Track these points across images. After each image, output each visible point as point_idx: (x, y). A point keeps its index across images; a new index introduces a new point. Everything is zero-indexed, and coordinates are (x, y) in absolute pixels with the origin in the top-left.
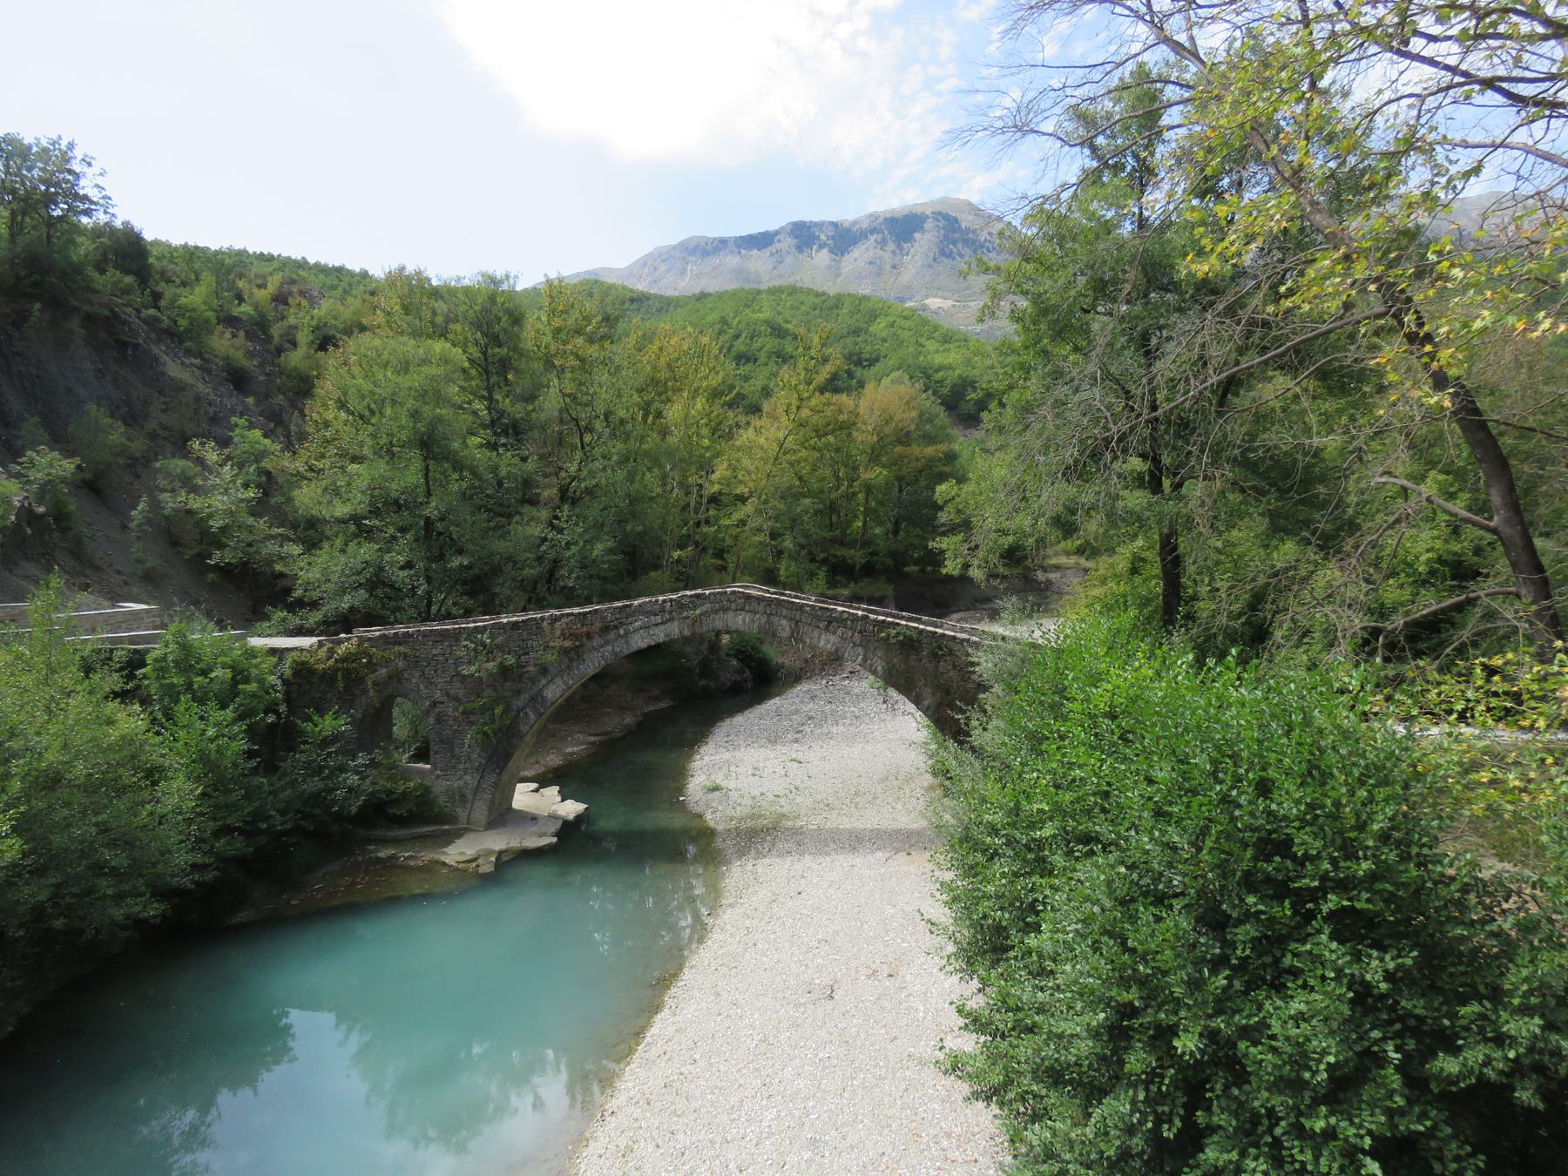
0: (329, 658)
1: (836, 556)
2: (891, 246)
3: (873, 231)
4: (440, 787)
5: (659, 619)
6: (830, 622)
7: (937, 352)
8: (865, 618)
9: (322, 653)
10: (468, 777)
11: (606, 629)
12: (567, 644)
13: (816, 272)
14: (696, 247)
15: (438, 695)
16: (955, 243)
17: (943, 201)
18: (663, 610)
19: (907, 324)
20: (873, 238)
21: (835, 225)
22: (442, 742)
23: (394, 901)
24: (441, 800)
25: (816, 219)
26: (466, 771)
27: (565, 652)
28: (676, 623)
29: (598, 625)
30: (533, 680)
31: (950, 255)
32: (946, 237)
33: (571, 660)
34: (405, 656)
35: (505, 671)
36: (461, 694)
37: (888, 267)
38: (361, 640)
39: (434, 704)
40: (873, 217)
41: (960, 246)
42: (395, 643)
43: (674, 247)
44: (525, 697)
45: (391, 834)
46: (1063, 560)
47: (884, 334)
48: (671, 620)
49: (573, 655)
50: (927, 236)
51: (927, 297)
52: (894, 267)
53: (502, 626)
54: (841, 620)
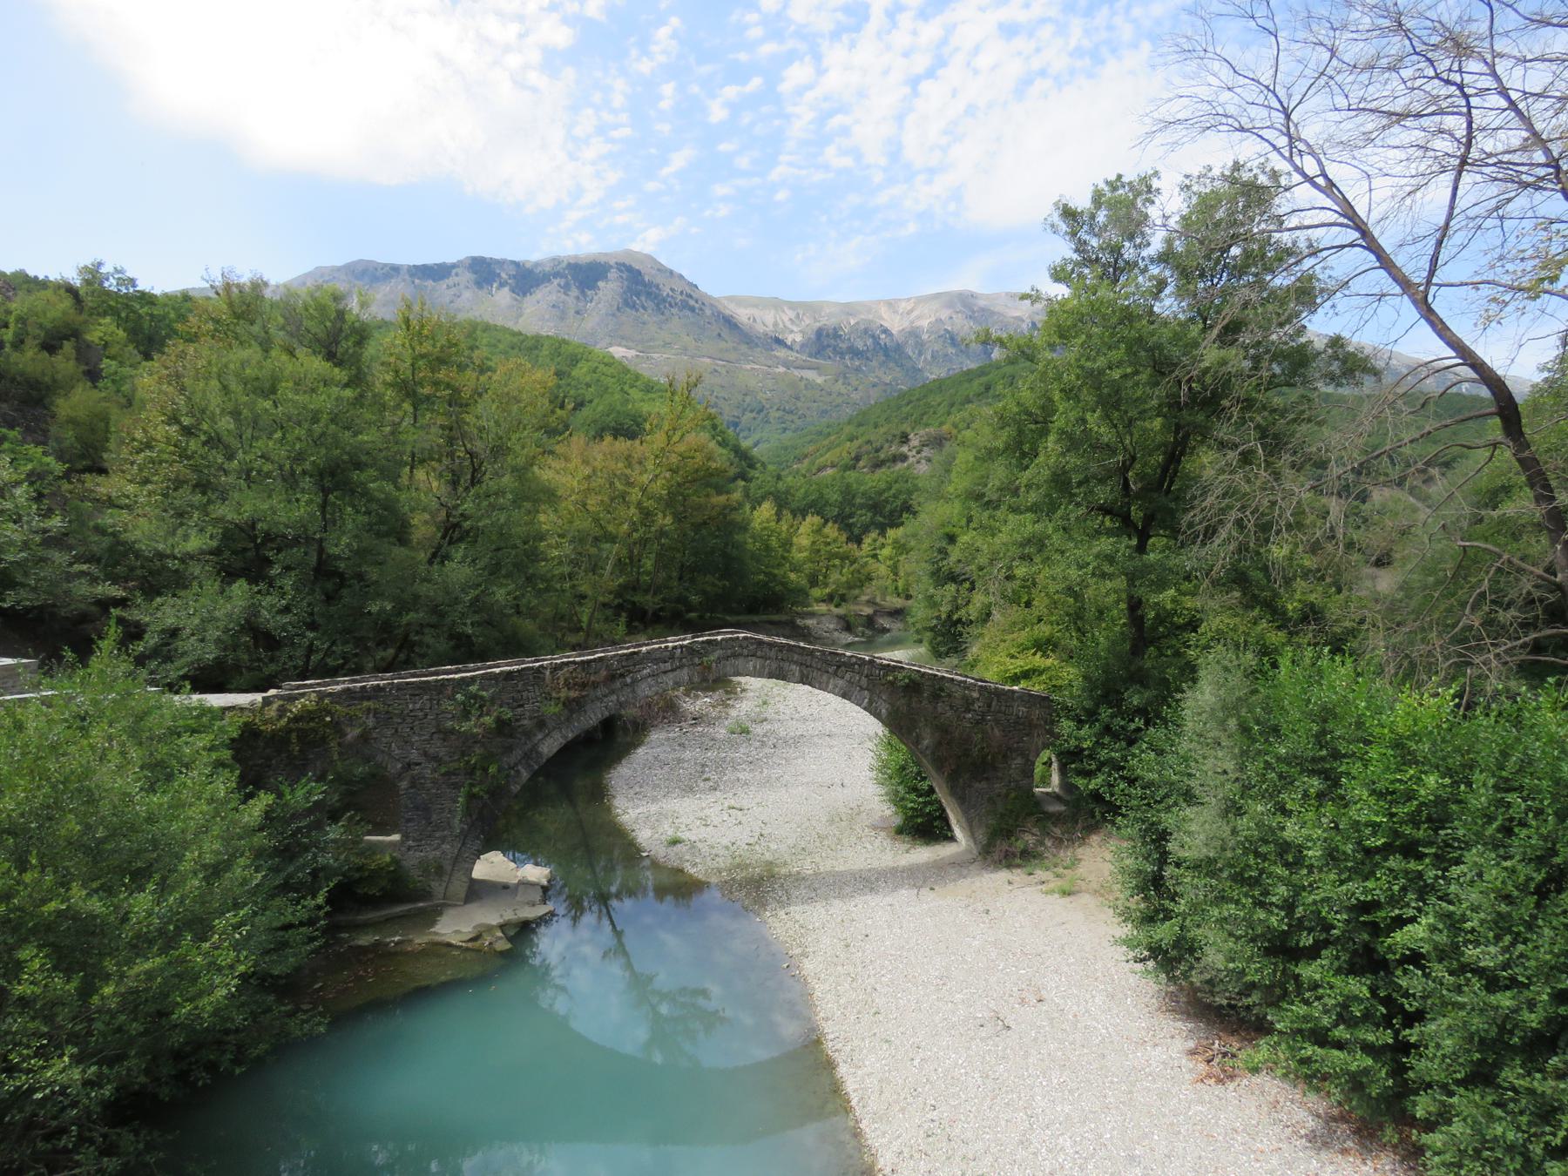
0: (280, 717)
1: (634, 603)
2: (575, 292)
3: (556, 275)
4: (411, 860)
5: (668, 666)
9: (272, 712)
10: (446, 847)
11: (612, 678)
12: (573, 694)
13: (496, 307)
14: (364, 272)
15: (414, 755)
16: (638, 295)
18: (672, 657)
19: (610, 371)
20: (556, 282)
22: (417, 808)
23: (422, 994)
24: (415, 874)
25: (497, 255)
26: (443, 839)
28: (685, 670)
29: (604, 673)
30: (528, 734)
31: (633, 307)
33: (572, 711)
34: (376, 712)
35: (503, 726)
36: (442, 752)
37: (572, 312)
39: (409, 766)
40: (556, 261)
42: (363, 698)
43: (339, 269)
44: (518, 754)
45: (362, 917)
46: (823, 608)
47: (588, 379)
48: (681, 667)
49: (574, 707)
50: (611, 285)
51: (611, 345)
52: (577, 313)
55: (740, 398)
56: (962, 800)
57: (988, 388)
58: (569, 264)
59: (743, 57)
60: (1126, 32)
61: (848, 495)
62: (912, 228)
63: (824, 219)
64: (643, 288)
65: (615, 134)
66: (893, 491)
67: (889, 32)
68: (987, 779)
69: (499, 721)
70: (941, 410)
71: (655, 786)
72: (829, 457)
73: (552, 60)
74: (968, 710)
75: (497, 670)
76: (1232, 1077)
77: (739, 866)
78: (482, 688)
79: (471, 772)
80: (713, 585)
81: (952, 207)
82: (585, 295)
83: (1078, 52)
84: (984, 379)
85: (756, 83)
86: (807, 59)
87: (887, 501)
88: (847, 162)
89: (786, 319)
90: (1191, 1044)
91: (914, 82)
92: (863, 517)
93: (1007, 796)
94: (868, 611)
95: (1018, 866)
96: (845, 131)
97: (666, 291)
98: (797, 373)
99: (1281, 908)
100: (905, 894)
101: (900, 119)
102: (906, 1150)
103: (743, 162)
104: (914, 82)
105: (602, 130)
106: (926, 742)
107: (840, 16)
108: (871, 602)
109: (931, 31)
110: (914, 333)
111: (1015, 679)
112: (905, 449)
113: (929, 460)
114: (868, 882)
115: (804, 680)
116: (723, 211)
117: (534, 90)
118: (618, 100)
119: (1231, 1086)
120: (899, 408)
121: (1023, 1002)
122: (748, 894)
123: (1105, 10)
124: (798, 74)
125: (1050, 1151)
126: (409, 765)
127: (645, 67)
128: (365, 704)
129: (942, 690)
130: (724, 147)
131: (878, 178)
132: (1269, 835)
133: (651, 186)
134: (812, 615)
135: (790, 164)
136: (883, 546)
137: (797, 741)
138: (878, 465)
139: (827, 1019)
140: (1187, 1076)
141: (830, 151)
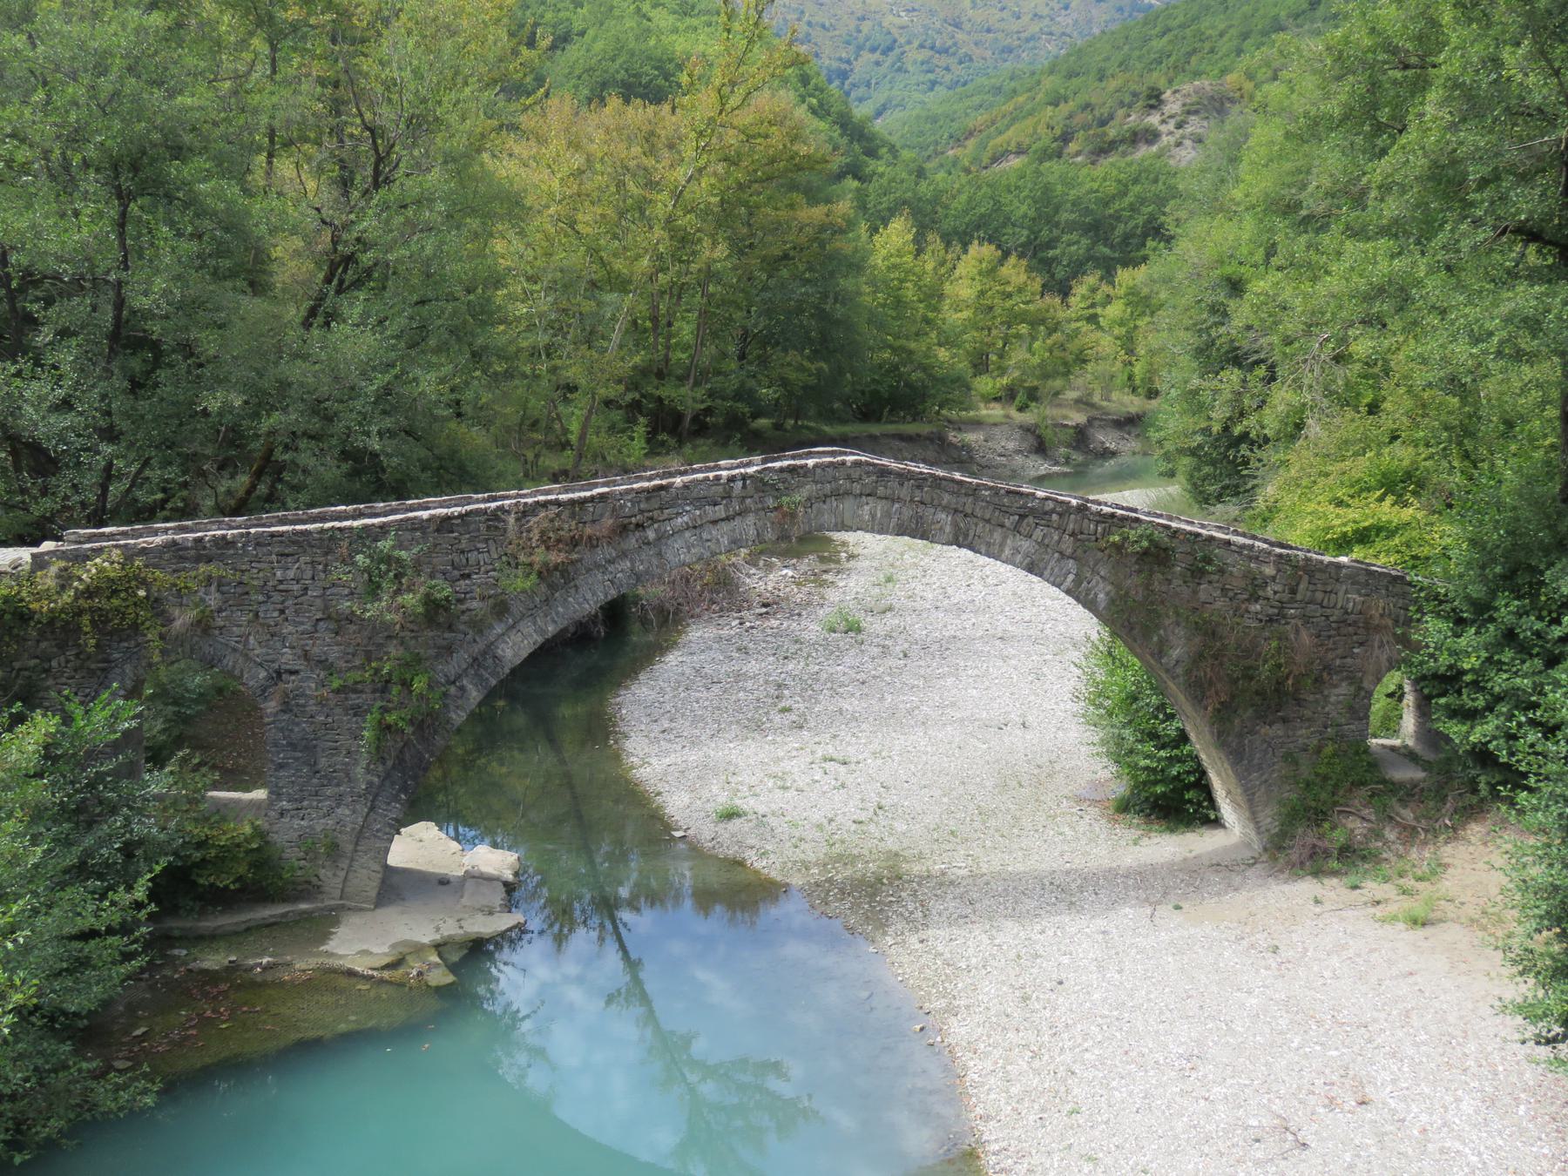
4: (286, 834)
5: (720, 511)
6: (1022, 517)
7: (675, 31)
9: (48, 579)
10: (343, 811)
11: (623, 530)
12: (556, 557)
15: (288, 658)
22: (293, 746)
24: (292, 855)
27: (546, 573)
29: (608, 522)
30: (479, 626)
33: (553, 587)
35: (435, 612)
36: (334, 653)
38: (130, 554)
42: (198, 559)
44: (461, 658)
46: (995, 412)
48: (741, 513)
49: (556, 579)
53: (420, 525)
56: (1237, 755)
68: (1285, 720)
70: (1225, 46)
71: (696, 720)
72: (1013, 135)
74: (1254, 598)
77: (839, 857)
79: (384, 687)
87: (1118, 218)
94: (1078, 418)
95: (1334, 873)
100: (1129, 914)
106: (1175, 653)
108: (1083, 403)
111: (1344, 544)
112: (1154, 119)
113: (1199, 140)
114: (1067, 892)
121: (1331, 1103)
126: (279, 673)
129: (1208, 561)
134: (977, 424)
136: (1108, 299)
137: (944, 647)
138: (1103, 149)
139: (986, 1118)
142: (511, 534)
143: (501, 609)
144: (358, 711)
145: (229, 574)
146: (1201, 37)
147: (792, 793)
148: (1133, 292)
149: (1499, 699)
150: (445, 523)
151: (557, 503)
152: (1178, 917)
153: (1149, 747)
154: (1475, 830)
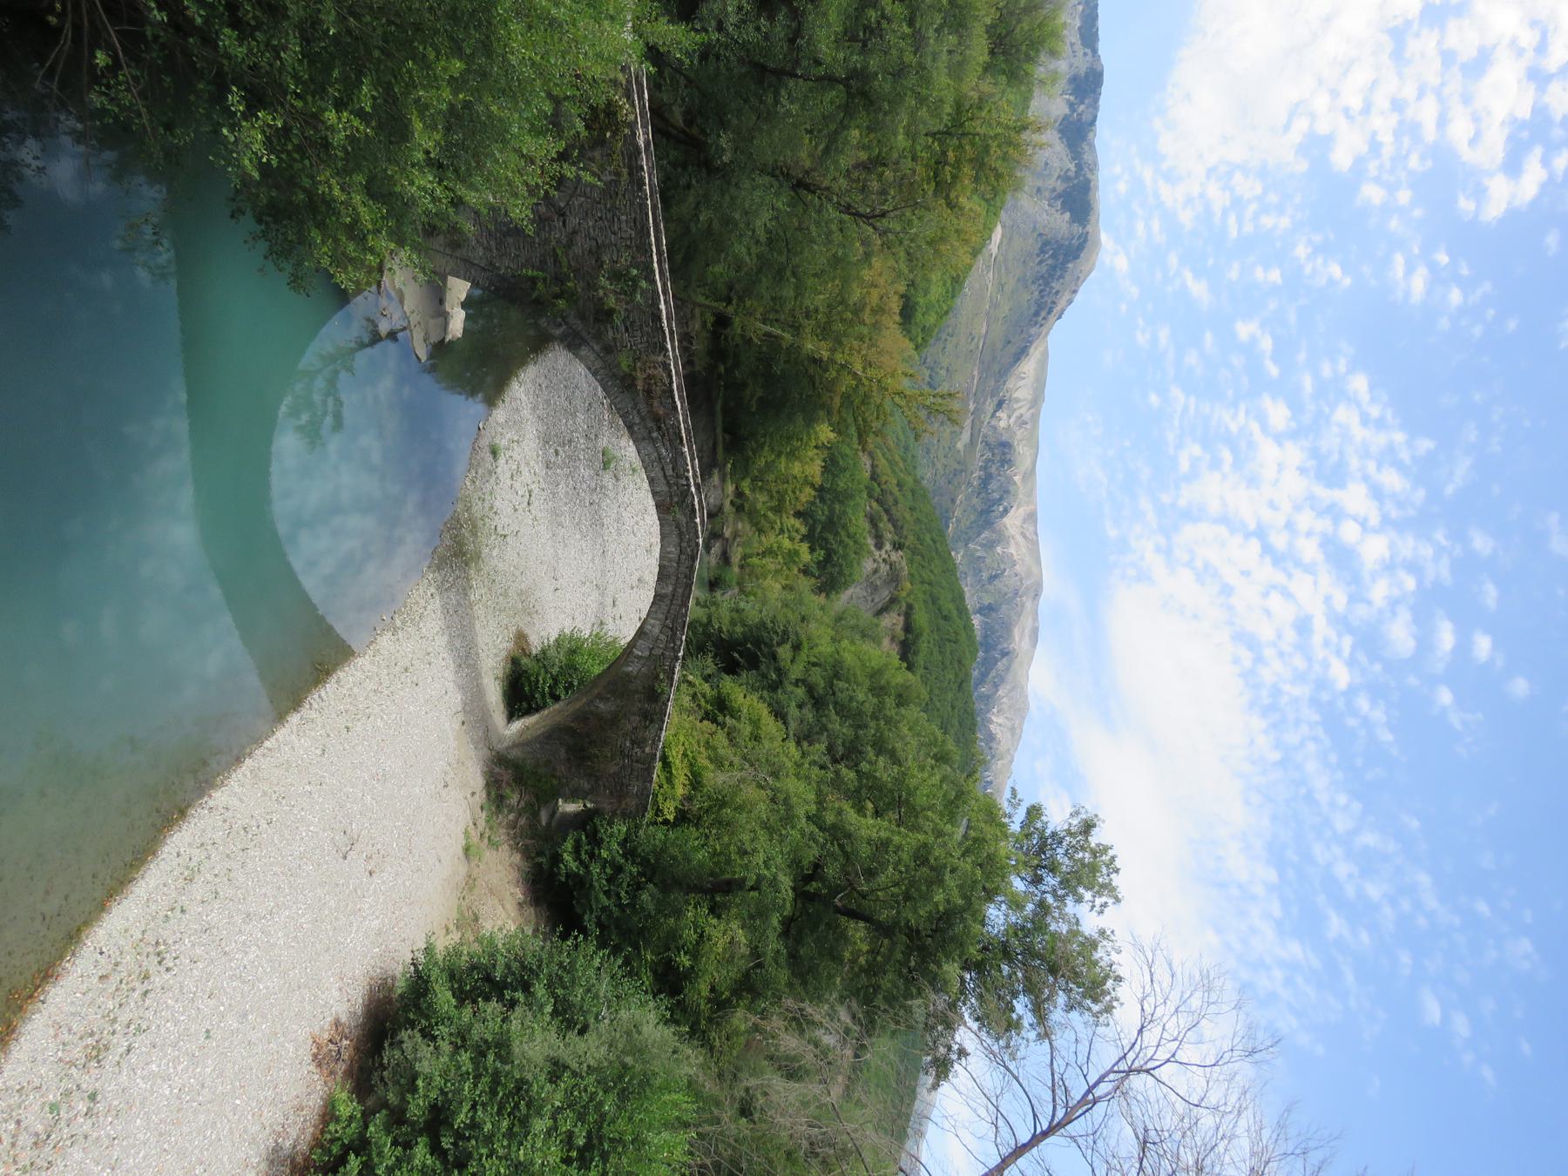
2: (1060, 186)
3: (1079, 167)
5: (670, 472)
8: (677, 658)
10: (481, 251)
11: (657, 420)
15: (573, 221)
16: (1054, 256)
17: (1097, 243)
18: (678, 476)
20: (1072, 167)
21: (1093, 122)
25: (1103, 101)
26: (487, 249)
28: (665, 488)
30: (598, 336)
31: (1042, 251)
32: (1060, 246)
33: (623, 379)
34: (617, 183)
36: (577, 250)
37: (1039, 184)
39: (562, 214)
41: (1050, 262)
42: (630, 168)
44: (578, 325)
46: (730, 488)
50: (1065, 226)
51: (1003, 227)
52: (1039, 190)
53: (656, 303)
54: (673, 638)
55: (945, 365)
56: (551, 736)
57: (946, 618)
58: (1089, 181)
59: (1302, 356)
60: (1292, 738)
61: (843, 497)
62: (1113, 533)
63: (1127, 443)
64: (1060, 261)
65: (1232, 219)
66: (846, 540)
67: (1312, 508)
68: (569, 760)
69: (611, 312)
70: (926, 574)
71: (547, 402)
72: (882, 463)
73: (1317, 146)
74: (633, 742)
75: (662, 306)
76: (319, 1065)
77: (475, 526)
78: (643, 292)
79: (559, 279)
80: (752, 396)
81: (1132, 572)
82: (1056, 198)
83: (1276, 691)
84: (955, 613)
85: (1274, 371)
86: (1293, 425)
87: (837, 534)
88: (1184, 466)
89: (1023, 411)
90: (344, 1019)
91: (1260, 533)
92: (821, 514)
93: (554, 776)
94: (727, 533)
95: (489, 794)
96: (1216, 464)
97: (1056, 285)
98: (968, 422)
99: (473, 1118)
100: (456, 699)
101: (1224, 520)
102: (229, 814)
103: (1192, 358)
104: (1260, 533)
105: (1237, 204)
106: (602, 706)
107: (1335, 457)
108: (736, 535)
109: (1310, 550)
110: (1001, 538)
111: (664, 759)
112: (888, 547)
113: (876, 571)
114: (466, 660)
115: (658, 597)
116: (1142, 339)
117: (1287, 127)
118: (1267, 221)
119: (312, 1068)
120: (929, 531)
121: (369, 858)
122: (448, 548)
123: (1316, 718)
124: (1279, 414)
125: (244, 944)
126: (563, 215)
127: (1301, 251)
128: (625, 171)
129: (652, 721)
130: (1208, 337)
131: (1166, 499)
132: (535, 1107)
133: (1173, 260)
134: (723, 480)
135: (1186, 409)
136: (791, 539)
137: (597, 523)
138: (873, 521)
139: (338, 682)
140: (317, 1028)
141: (1197, 450)
142: (653, 358)
143: (608, 350)
144: (543, 262)
145: (623, 187)
146: (931, 560)
147: (509, 482)
148: (797, 553)
149: (587, 867)
150: (657, 317)
151: (671, 382)
152: (457, 726)
153: (550, 682)
154: (517, 858)
